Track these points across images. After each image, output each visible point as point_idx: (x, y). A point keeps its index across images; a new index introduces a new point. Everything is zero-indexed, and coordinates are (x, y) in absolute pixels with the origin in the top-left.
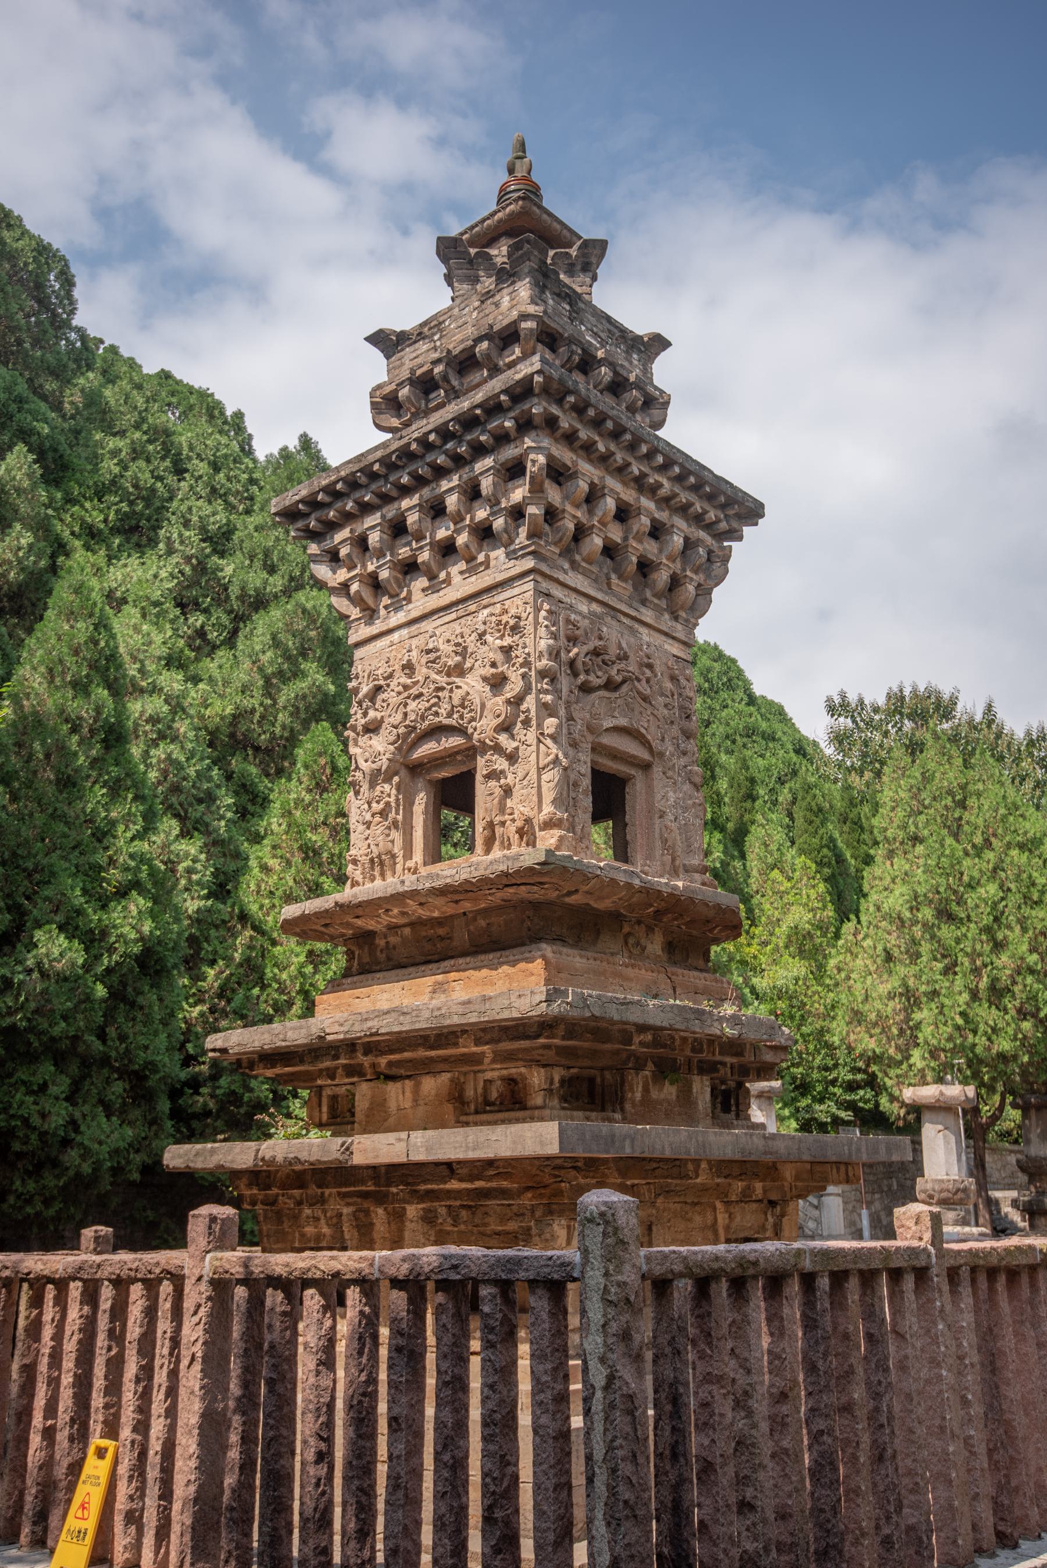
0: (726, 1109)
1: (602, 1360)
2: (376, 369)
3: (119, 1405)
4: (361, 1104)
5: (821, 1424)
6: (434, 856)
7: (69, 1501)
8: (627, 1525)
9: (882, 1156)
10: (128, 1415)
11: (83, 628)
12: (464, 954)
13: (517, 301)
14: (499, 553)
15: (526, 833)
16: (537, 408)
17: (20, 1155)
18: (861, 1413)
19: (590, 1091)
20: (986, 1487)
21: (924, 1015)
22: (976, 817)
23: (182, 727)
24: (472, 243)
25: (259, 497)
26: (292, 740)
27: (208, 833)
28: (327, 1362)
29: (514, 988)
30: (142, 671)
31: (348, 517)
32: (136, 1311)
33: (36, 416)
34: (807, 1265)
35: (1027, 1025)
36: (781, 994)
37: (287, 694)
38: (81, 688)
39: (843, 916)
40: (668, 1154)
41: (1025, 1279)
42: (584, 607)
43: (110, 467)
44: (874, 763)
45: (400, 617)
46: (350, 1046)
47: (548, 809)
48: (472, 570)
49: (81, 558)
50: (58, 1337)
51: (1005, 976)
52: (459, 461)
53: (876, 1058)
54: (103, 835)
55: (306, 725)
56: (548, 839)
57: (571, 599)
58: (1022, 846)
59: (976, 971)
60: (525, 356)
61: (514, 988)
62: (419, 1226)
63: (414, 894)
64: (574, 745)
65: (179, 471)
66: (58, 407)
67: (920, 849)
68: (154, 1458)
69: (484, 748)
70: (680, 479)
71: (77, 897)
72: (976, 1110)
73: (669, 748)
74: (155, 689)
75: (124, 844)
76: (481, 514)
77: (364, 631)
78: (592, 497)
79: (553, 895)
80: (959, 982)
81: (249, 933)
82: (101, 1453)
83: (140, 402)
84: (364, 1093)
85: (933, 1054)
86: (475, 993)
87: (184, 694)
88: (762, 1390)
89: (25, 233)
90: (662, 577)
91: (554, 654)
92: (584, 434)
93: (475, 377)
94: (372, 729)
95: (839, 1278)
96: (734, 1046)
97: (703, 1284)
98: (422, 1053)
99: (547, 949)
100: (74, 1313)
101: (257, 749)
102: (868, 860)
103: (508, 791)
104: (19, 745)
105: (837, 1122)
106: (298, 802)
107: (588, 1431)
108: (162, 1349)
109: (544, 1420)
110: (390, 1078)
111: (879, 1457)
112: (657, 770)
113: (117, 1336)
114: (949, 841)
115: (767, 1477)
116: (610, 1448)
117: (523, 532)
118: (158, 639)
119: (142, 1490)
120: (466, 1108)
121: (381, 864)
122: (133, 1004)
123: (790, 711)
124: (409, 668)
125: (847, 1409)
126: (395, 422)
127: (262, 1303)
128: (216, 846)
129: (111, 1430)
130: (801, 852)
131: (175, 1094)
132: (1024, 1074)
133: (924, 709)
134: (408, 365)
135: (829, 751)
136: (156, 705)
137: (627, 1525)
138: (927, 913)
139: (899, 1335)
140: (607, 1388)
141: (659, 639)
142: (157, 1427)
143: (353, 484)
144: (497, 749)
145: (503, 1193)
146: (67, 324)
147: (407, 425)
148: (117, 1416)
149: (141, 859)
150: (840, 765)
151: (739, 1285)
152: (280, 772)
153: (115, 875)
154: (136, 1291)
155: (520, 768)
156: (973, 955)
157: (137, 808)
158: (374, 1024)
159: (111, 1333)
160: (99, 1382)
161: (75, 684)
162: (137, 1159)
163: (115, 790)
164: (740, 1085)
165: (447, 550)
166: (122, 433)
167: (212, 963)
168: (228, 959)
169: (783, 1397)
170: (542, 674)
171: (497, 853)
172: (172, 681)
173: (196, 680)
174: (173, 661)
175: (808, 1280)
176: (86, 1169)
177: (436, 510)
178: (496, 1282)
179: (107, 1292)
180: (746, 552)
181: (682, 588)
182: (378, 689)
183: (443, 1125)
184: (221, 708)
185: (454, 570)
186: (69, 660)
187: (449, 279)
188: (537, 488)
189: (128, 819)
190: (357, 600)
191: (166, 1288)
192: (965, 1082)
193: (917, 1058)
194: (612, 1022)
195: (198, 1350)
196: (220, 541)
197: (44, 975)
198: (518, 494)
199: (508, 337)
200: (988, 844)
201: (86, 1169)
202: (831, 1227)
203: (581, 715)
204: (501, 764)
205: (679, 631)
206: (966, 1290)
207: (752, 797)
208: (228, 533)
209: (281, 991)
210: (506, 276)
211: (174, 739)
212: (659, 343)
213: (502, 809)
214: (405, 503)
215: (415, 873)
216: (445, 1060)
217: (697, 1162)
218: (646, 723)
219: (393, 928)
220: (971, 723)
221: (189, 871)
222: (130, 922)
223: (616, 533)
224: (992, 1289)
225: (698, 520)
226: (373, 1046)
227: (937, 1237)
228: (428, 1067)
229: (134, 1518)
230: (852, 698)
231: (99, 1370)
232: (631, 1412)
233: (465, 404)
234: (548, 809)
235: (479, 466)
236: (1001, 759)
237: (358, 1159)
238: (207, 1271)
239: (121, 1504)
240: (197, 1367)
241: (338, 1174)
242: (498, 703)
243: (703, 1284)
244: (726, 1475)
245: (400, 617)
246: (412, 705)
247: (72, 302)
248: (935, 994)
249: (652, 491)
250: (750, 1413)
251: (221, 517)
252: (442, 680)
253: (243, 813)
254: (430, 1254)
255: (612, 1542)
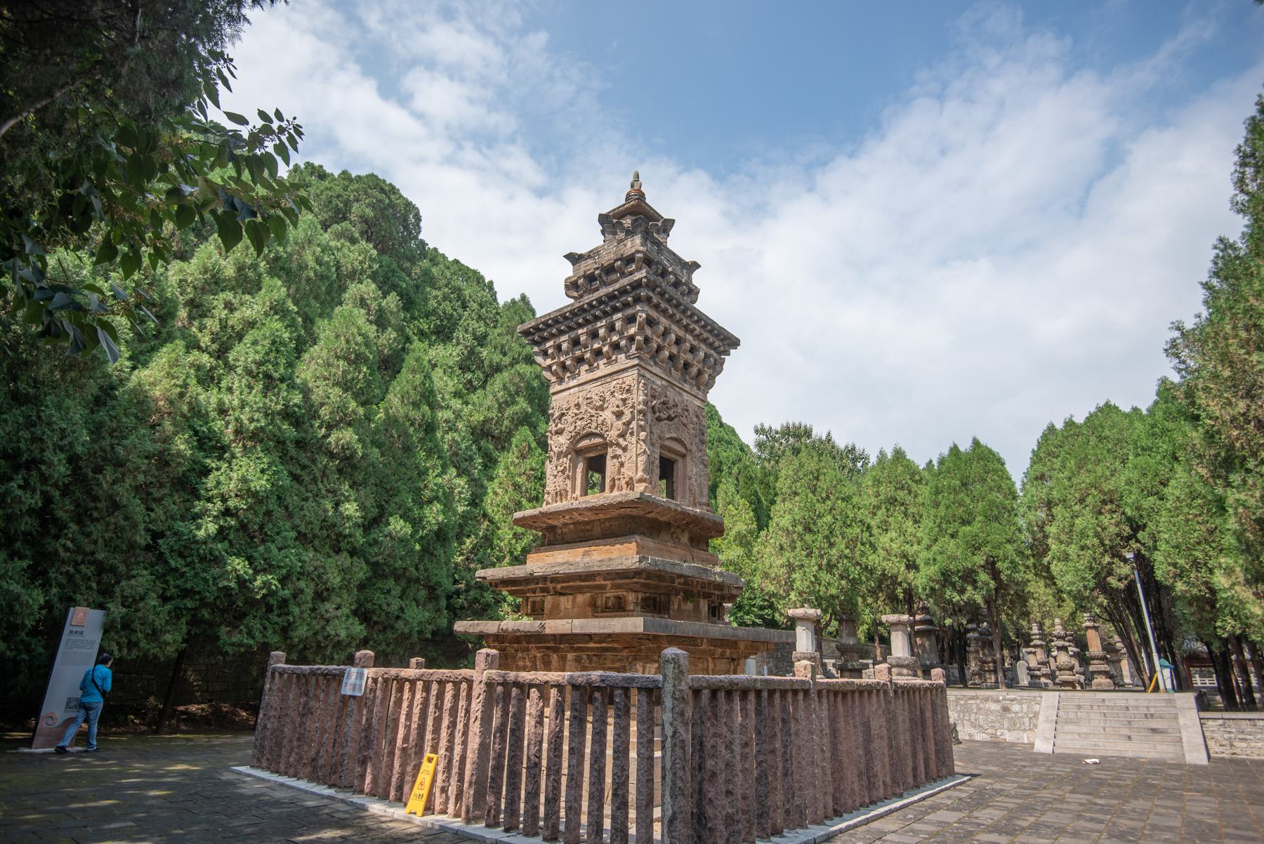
0: (714, 615)
1: (671, 724)
2: (568, 270)
3: (439, 738)
4: (547, 606)
5: (762, 758)
6: (585, 493)
7: (414, 782)
8: (680, 798)
9: (784, 640)
10: (443, 743)
11: (419, 378)
12: (598, 538)
13: (635, 244)
14: (623, 356)
15: (630, 484)
16: (643, 293)
17: (376, 623)
18: (779, 754)
19: (654, 605)
20: (830, 790)
21: (796, 575)
22: (823, 484)
23: (460, 425)
24: (614, 217)
25: (501, 321)
26: (510, 434)
27: (469, 475)
28: (540, 722)
29: (623, 555)
30: (443, 398)
31: (553, 336)
32: (448, 696)
33: (400, 278)
34: (759, 686)
35: (843, 582)
36: (731, 563)
37: (509, 412)
38: (416, 405)
39: (760, 528)
40: (691, 634)
41: (849, 697)
42: (659, 382)
43: (433, 303)
44: (776, 457)
45: (574, 382)
46: (544, 578)
47: (640, 474)
48: (609, 363)
49: (417, 344)
50: (410, 706)
51: (834, 560)
52: (606, 314)
53: (774, 595)
54: (422, 473)
55: (516, 426)
56: (640, 488)
57: (654, 379)
58: (843, 499)
59: (821, 556)
60: (639, 269)
61: (623, 555)
62: (574, 664)
63: (577, 509)
64: (653, 444)
65: (464, 307)
66: (409, 275)
67: (797, 498)
68: (456, 764)
69: (612, 444)
70: (704, 327)
71: (410, 503)
72: (819, 621)
73: (694, 448)
74: (448, 407)
75: (434, 479)
76: (615, 338)
77: (558, 388)
78: (666, 333)
79: (642, 513)
80: (813, 561)
81: (486, 523)
82: (430, 760)
83: (448, 275)
84: (549, 600)
85: (800, 594)
86: (604, 557)
87: (461, 410)
88: (738, 741)
89: (401, 196)
90: (694, 370)
91: (645, 403)
92: (663, 305)
93: (614, 277)
94: (559, 432)
95: (771, 693)
96: (720, 586)
97: (714, 693)
98: (578, 583)
99: (638, 538)
100: (419, 696)
101: (493, 437)
102: (773, 502)
103: (622, 465)
104: (387, 430)
105: (754, 624)
106: (512, 463)
107: (663, 757)
108: (461, 713)
109: (643, 751)
110: (561, 594)
111: (786, 775)
112: (688, 458)
113: (439, 707)
114: (810, 495)
115: (739, 779)
116: (673, 763)
117: (634, 347)
118: (451, 384)
119: (449, 778)
120: (597, 610)
121: (561, 495)
122: (432, 554)
123: (738, 431)
124: (578, 406)
125: (773, 751)
126: (576, 294)
127: (510, 695)
128: (473, 482)
129: (435, 749)
130: (742, 497)
131: (449, 597)
132: (841, 604)
133: (798, 433)
134: (583, 269)
135: (755, 450)
136: (448, 414)
137: (680, 798)
138: (800, 528)
139: (796, 720)
140: (673, 737)
141: (691, 398)
142: (458, 749)
143: (556, 321)
144: (618, 445)
145: (614, 649)
146: (416, 238)
147: (581, 296)
148: (437, 744)
149: (440, 486)
150: (760, 458)
151: (729, 693)
152: (503, 448)
153: (427, 493)
154: (449, 686)
155: (628, 454)
156: (820, 549)
157: (439, 462)
158: (557, 569)
159: (436, 705)
160: (430, 727)
161: (413, 403)
162: (430, 627)
163: (430, 453)
164: (720, 604)
165: (598, 353)
166: (439, 289)
167: (468, 536)
168: (476, 535)
169: (746, 745)
170: (640, 412)
171: (616, 493)
172: (456, 404)
173: (467, 403)
174: (457, 394)
175: (758, 693)
176: (406, 631)
177: (594, 335)
178: (622, 688)
179: (435, 687)
180: (732, 361)
181: (703, 378)
182: (563, 414)
183: (586, 617)
184: (478, 417)
185: (601, 363)
186: (412, 392)
187: (603, 232)
188: (641, 328)
189: (434, 467)
190: (554, 373)
191: (464, 686)
192: (814, 607)
193: (793, 596)
194: (667, 572)
195: (479, 714)
196: (481, 340)
197: (392, 538)
198: (632, 331)
199: (630, 260)
200: (828, 497)
201: (406, 631)
202: (752, 671)
203: (656, 431)
204: (619, 452)
205: (700, 395)
206: (825, 701)
207: (720, 470)
208: (485, 336)
209: (500, 551)
210: (630, 233)
211: (456, 431)
212: (695, 266)
213: (619, 473)
214: (580, 331)
215: (577, 500)
216: (588, 587)
217: (702, 639)
218: (681, 438)
219: (565, 525)
220: (820, 440)
221: (460, 493)
222: (434, 515)
223: (674, 350)
224: (835, 701)
225: (711, 345)
226: (555, 579)
227: (813, 678)
228: (580, 590)
229: (444, 790)
230: (766, 427)
231: (430, 722)
232: (683, 748)
233: (611, 289)
234: (640, 474)
235: (615, 317)
236: (834, 458)
237: (547, 631)
238: (484, 679)
239: (439, 783)
240: (478, 722)
241: (537, 638)
242: (619, 424)
243: (714, 693)
244: (721, 778)
245: (574, 382)
246: (579, 423)
247: (419, 228)
248: (802, 566)
249: (692, 332)
250: (732, 751)
251: (483, 329)
252: (593, 412)
253: (485, 466)
254: (595, 675)
255: (673, 806)
